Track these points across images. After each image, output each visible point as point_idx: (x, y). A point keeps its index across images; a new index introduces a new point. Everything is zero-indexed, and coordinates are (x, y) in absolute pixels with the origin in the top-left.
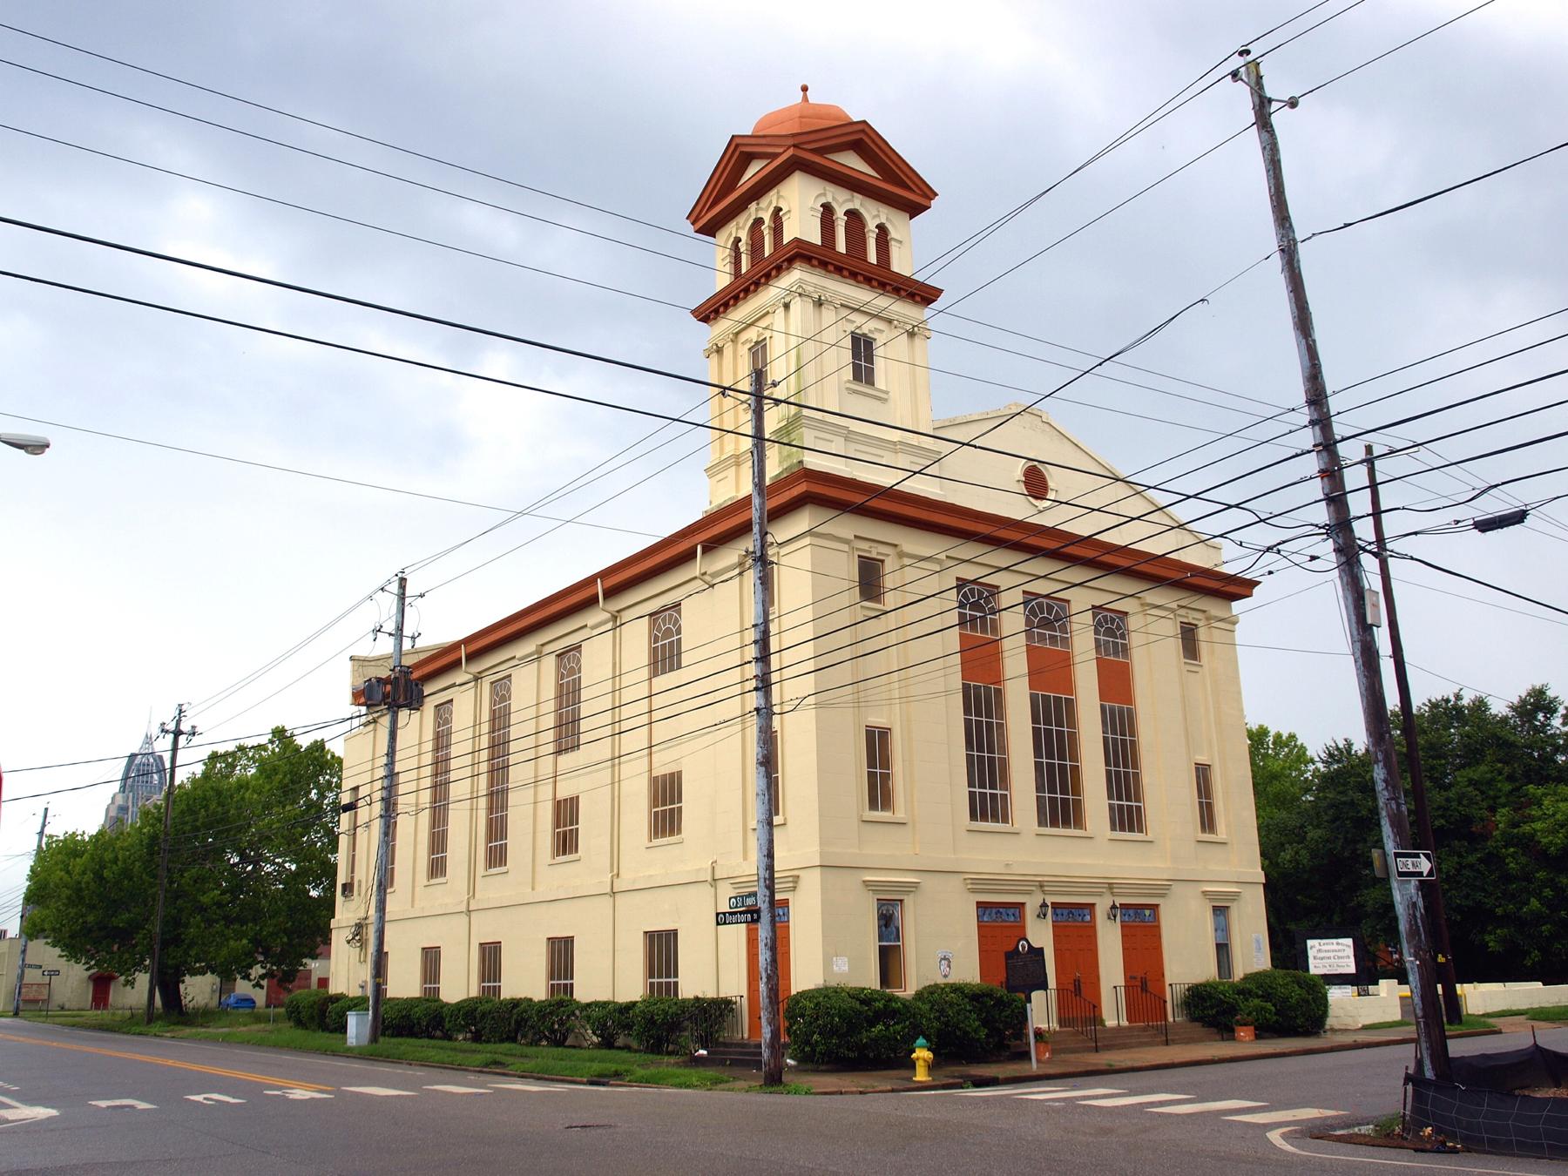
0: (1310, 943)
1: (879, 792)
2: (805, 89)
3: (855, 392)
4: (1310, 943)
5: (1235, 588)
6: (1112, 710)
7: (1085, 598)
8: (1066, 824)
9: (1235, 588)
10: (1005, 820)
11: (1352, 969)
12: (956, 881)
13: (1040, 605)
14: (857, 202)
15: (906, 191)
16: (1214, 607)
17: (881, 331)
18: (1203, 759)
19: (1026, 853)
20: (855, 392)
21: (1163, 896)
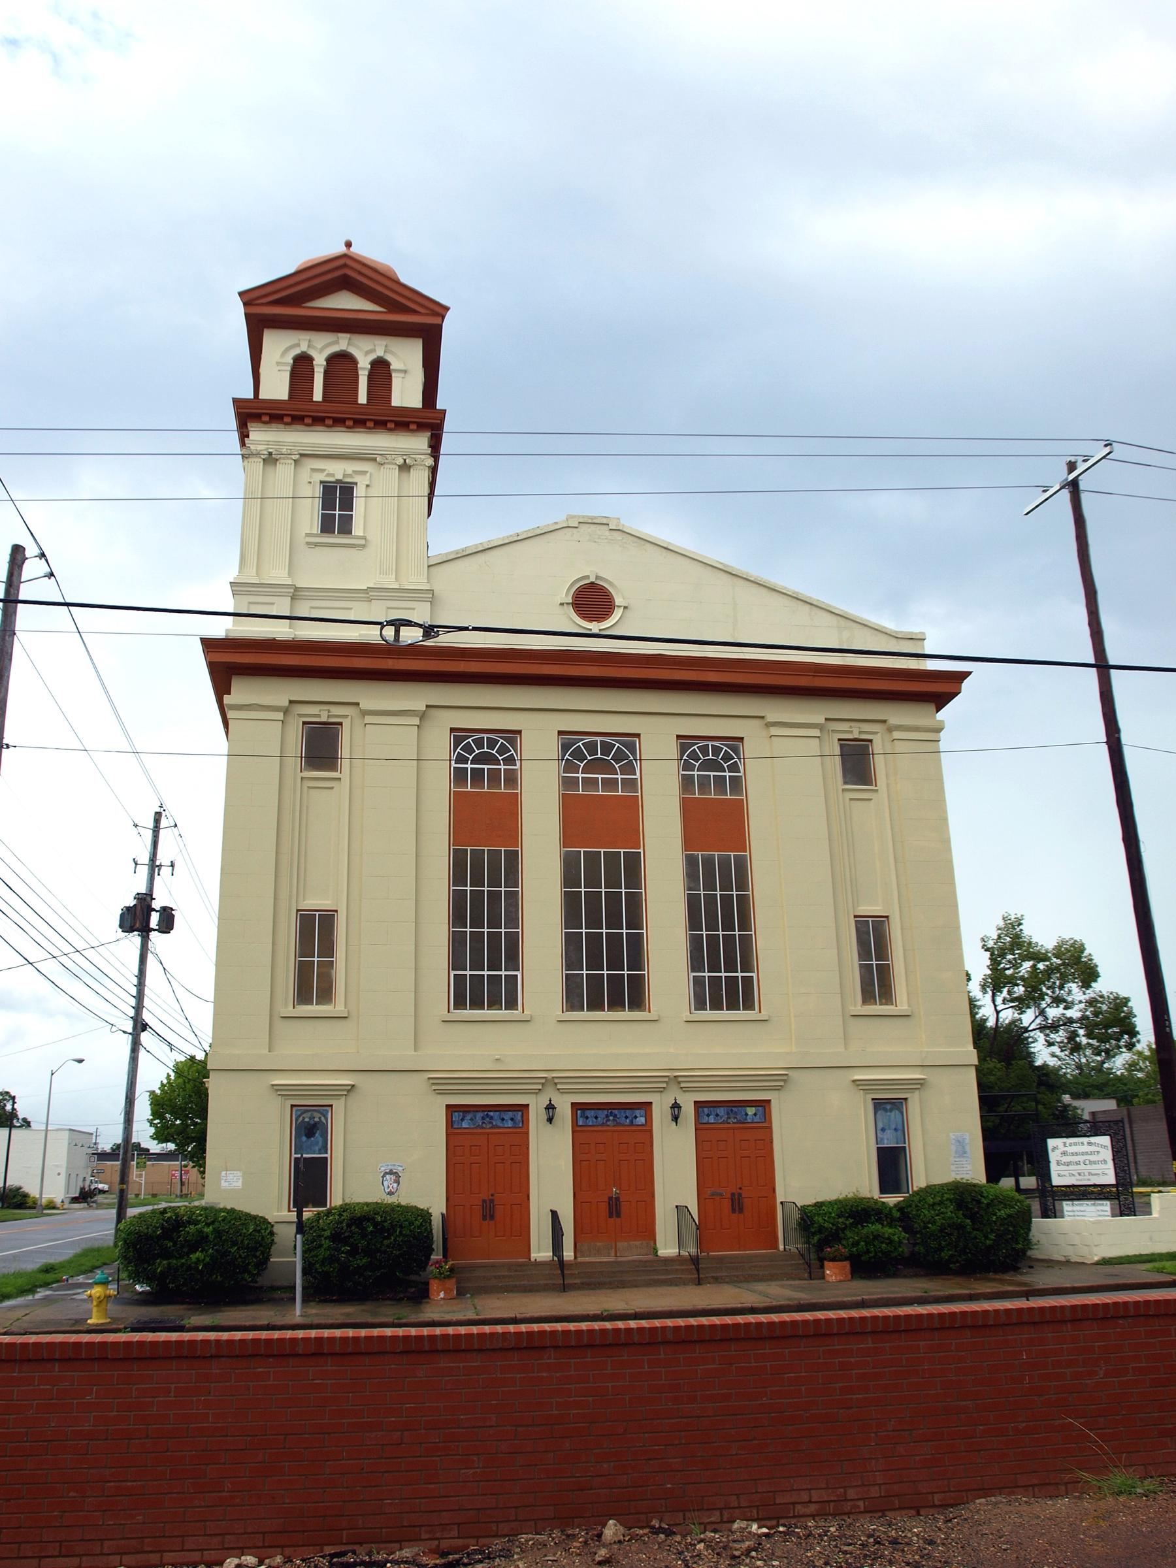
0: (1051, 1143)
1: (313, 982)
3: (317, 545)
4: (1051, 1143)
5: (936, 689)
6: (708, 863)
7: (659, 733)
8: (733, 1006)
9: (936, 689)
10: (749, 1006)
11: (1110, 1179)
12: (420, 1080)
14: (342, 342)
15: (418, 319)
16: (898, 714)
17: (364, 473)
18: (315, 902)
19: (545, 1042)
20: (317, 545)
21: (778, 1089)
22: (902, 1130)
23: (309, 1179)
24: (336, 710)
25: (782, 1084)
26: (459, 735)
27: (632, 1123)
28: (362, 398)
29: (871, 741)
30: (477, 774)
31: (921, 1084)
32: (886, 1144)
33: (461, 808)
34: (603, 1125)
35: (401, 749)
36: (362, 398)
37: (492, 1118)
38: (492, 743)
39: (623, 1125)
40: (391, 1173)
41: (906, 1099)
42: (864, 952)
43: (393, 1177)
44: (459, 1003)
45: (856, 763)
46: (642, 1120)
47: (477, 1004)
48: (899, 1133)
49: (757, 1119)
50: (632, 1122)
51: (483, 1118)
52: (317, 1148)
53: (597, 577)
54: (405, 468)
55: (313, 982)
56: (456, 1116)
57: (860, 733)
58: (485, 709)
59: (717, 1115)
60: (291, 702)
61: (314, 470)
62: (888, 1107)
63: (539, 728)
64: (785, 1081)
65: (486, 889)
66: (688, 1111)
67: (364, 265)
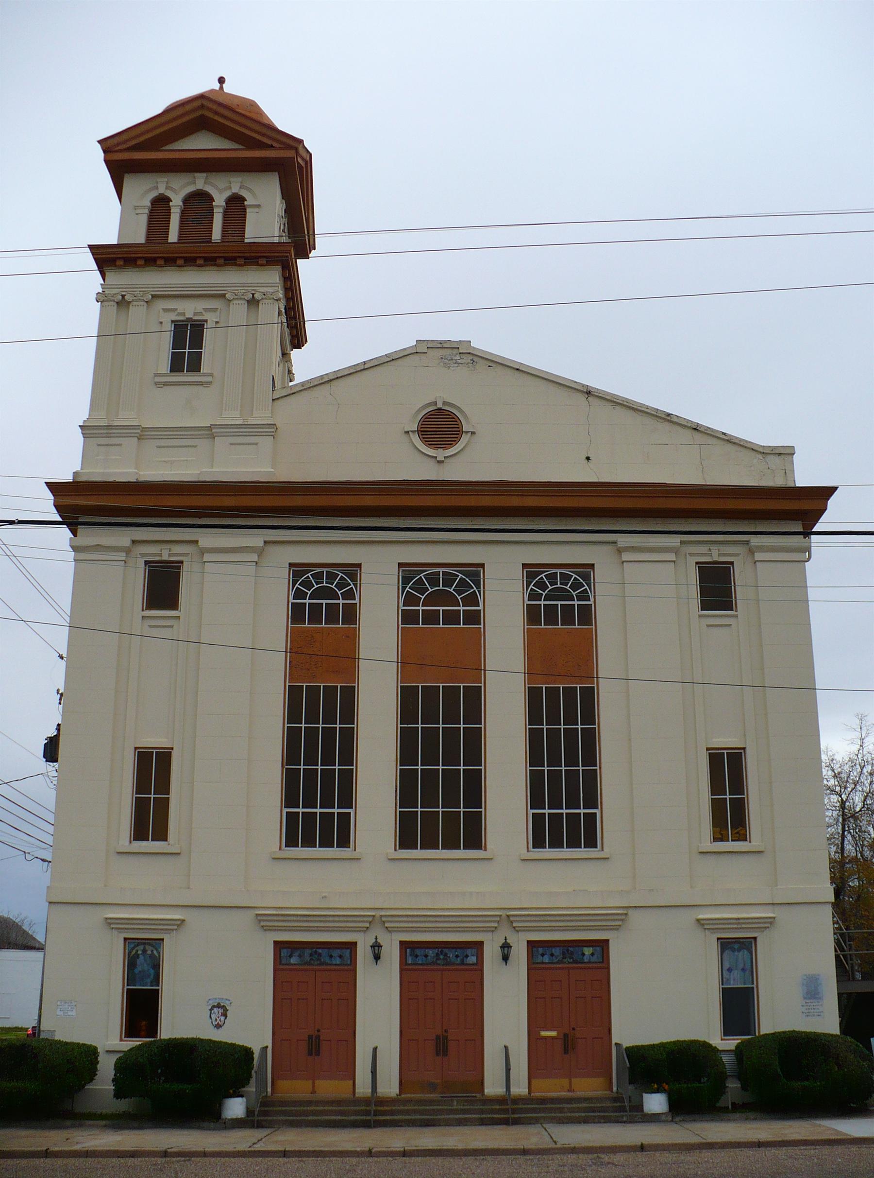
1: (150, 819)
2: (221, 80)
3: (166, 384)
7: (504, 570)
13: (552, 578)
14: (199, 182)
17: (214, 310)
19: (375, 881)
20: (166, 384)
21: (617, 928)
22: (750, 970)
23: (142, 1008)
24: (177, 549)
25: (619, 923)
26: (298, 570)
27: (462, 963)
28: (217, 235)
29: (732, 563)
30: (315, 610)
31: (771, 923)
32: (732, 985)
33: (296, 702)
34: (433, 963)
35: (241, 592)
36: (217, 235)
37: (320, 955)
38: (331, 577)
39: (454, 964)
40: (219, 1006)
41: (755, 938)
42: (716, 786)
43: (221, 1011)
44: (291, 841)
45: (716, 589)
46: (473, 959)
47: (309, 842)
48: (748, 973)
49: (594, 959)
50: (463, 960)
51: (311, 955)
52: (149, 980)
53: (445, 403)
54: (253, 302)
55: (150, 819)
56: (285, 952)
57: (719, 555)
58: (325, 549)
59: (552, 955)
60: (134, 542)
61: (166, 310)
62: (736, 946)
63: (380, 569)
64: (622, 920)
65: (321, 726)
66: (520, 953)
67: (220, 104)
